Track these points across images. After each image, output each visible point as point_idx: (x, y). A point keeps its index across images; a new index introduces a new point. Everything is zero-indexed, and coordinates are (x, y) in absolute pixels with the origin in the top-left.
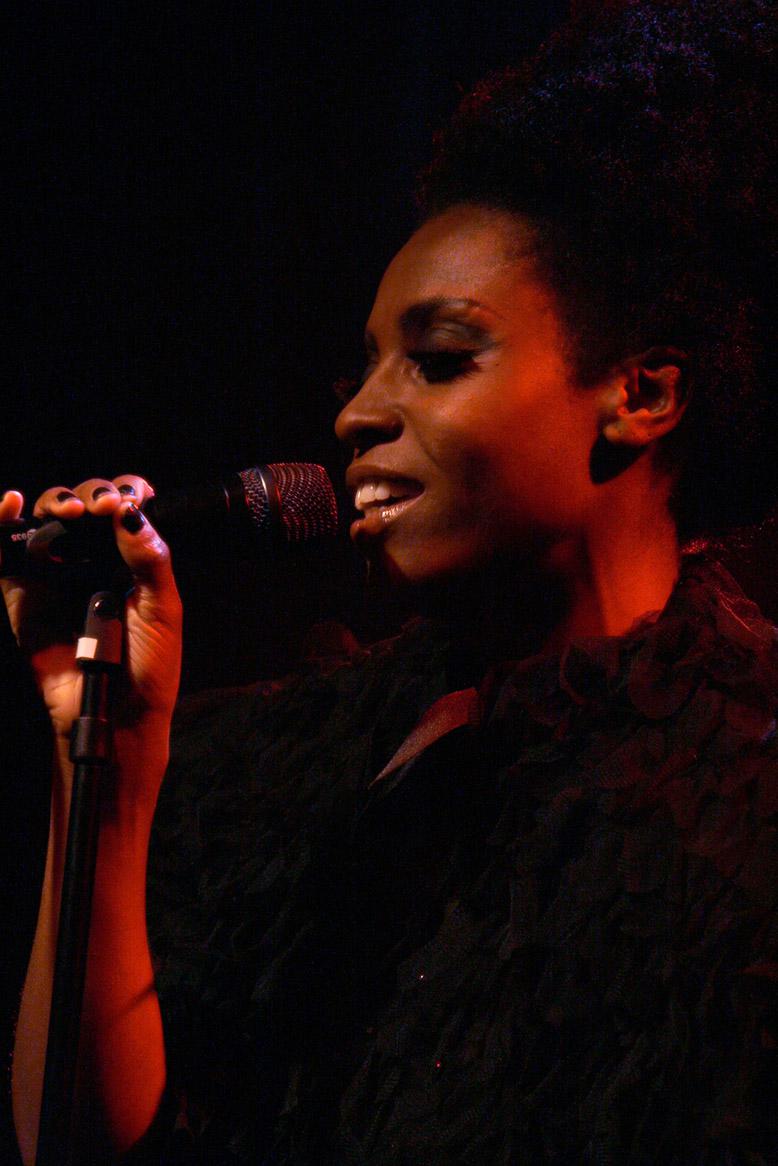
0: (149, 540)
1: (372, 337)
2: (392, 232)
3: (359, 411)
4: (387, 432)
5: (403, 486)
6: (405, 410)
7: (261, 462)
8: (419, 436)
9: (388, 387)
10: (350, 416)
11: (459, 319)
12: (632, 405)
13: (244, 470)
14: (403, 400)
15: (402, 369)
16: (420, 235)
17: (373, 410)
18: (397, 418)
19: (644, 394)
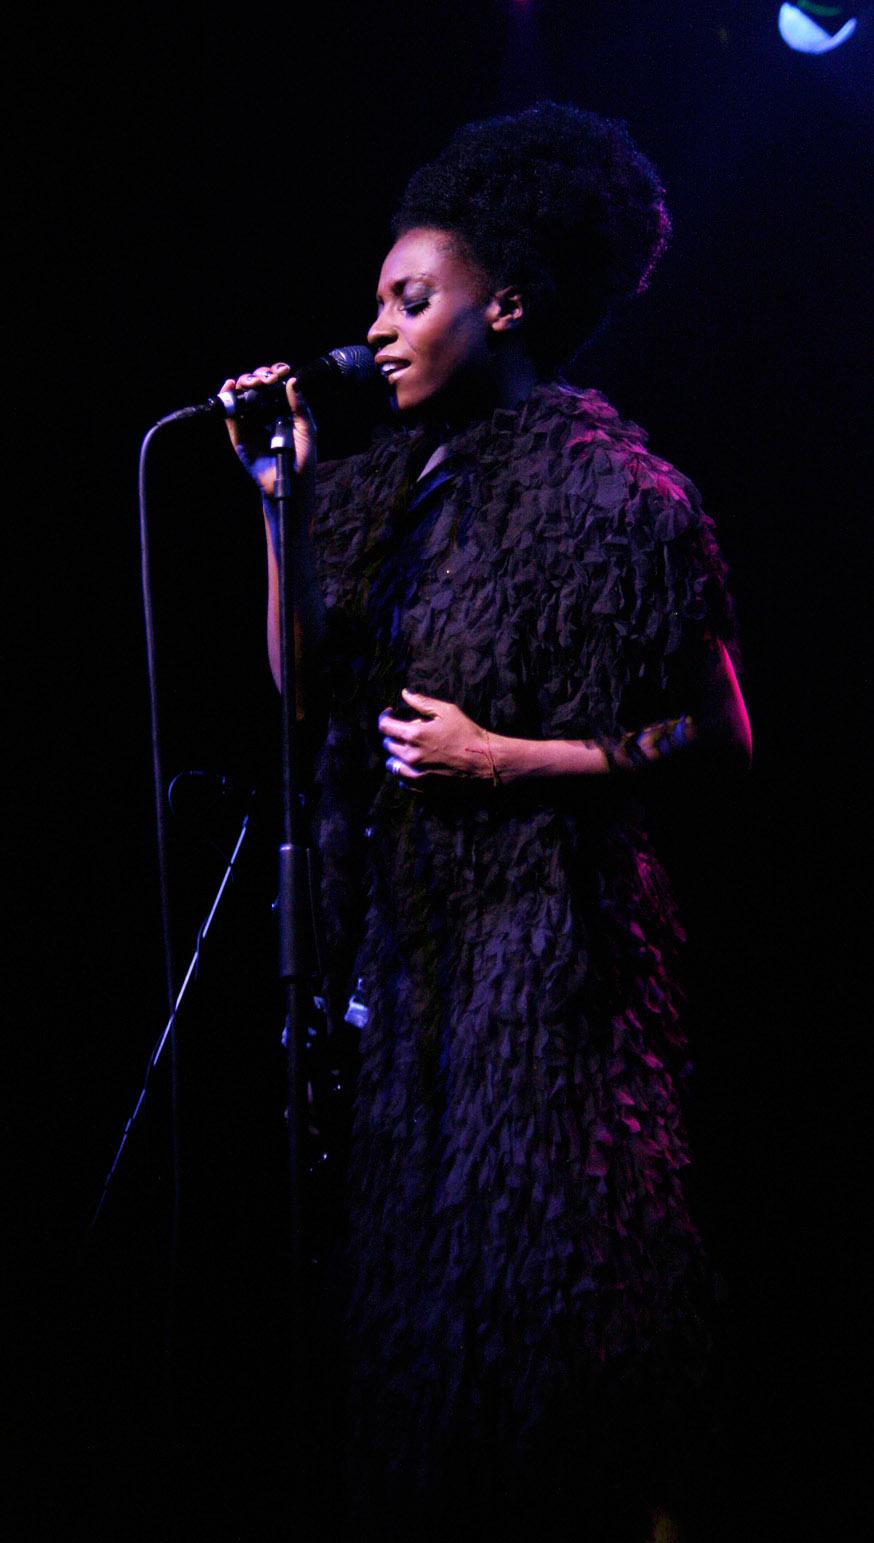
0: (242, 451)
1: (380, 297)
2: (384, 245)
3: (377, 329)
4: (390, 339)
5: (402, 363)
6: (398, 327)
7: (340, 346)
8: (407, 339)
9: (390, 318)
10: (373, 332)
11: (555, 919)
12: (502, 314)
13: (331, 350)
14: (356, 497)
15: (395, 308)
16: (400, 243)
17: (384, 329)
18: (395, 331)
19: (507, 308)
